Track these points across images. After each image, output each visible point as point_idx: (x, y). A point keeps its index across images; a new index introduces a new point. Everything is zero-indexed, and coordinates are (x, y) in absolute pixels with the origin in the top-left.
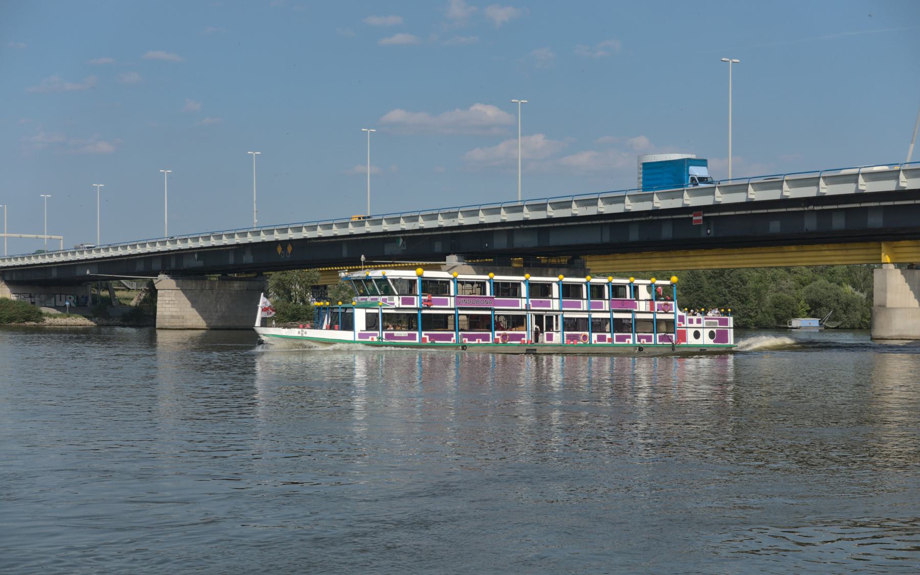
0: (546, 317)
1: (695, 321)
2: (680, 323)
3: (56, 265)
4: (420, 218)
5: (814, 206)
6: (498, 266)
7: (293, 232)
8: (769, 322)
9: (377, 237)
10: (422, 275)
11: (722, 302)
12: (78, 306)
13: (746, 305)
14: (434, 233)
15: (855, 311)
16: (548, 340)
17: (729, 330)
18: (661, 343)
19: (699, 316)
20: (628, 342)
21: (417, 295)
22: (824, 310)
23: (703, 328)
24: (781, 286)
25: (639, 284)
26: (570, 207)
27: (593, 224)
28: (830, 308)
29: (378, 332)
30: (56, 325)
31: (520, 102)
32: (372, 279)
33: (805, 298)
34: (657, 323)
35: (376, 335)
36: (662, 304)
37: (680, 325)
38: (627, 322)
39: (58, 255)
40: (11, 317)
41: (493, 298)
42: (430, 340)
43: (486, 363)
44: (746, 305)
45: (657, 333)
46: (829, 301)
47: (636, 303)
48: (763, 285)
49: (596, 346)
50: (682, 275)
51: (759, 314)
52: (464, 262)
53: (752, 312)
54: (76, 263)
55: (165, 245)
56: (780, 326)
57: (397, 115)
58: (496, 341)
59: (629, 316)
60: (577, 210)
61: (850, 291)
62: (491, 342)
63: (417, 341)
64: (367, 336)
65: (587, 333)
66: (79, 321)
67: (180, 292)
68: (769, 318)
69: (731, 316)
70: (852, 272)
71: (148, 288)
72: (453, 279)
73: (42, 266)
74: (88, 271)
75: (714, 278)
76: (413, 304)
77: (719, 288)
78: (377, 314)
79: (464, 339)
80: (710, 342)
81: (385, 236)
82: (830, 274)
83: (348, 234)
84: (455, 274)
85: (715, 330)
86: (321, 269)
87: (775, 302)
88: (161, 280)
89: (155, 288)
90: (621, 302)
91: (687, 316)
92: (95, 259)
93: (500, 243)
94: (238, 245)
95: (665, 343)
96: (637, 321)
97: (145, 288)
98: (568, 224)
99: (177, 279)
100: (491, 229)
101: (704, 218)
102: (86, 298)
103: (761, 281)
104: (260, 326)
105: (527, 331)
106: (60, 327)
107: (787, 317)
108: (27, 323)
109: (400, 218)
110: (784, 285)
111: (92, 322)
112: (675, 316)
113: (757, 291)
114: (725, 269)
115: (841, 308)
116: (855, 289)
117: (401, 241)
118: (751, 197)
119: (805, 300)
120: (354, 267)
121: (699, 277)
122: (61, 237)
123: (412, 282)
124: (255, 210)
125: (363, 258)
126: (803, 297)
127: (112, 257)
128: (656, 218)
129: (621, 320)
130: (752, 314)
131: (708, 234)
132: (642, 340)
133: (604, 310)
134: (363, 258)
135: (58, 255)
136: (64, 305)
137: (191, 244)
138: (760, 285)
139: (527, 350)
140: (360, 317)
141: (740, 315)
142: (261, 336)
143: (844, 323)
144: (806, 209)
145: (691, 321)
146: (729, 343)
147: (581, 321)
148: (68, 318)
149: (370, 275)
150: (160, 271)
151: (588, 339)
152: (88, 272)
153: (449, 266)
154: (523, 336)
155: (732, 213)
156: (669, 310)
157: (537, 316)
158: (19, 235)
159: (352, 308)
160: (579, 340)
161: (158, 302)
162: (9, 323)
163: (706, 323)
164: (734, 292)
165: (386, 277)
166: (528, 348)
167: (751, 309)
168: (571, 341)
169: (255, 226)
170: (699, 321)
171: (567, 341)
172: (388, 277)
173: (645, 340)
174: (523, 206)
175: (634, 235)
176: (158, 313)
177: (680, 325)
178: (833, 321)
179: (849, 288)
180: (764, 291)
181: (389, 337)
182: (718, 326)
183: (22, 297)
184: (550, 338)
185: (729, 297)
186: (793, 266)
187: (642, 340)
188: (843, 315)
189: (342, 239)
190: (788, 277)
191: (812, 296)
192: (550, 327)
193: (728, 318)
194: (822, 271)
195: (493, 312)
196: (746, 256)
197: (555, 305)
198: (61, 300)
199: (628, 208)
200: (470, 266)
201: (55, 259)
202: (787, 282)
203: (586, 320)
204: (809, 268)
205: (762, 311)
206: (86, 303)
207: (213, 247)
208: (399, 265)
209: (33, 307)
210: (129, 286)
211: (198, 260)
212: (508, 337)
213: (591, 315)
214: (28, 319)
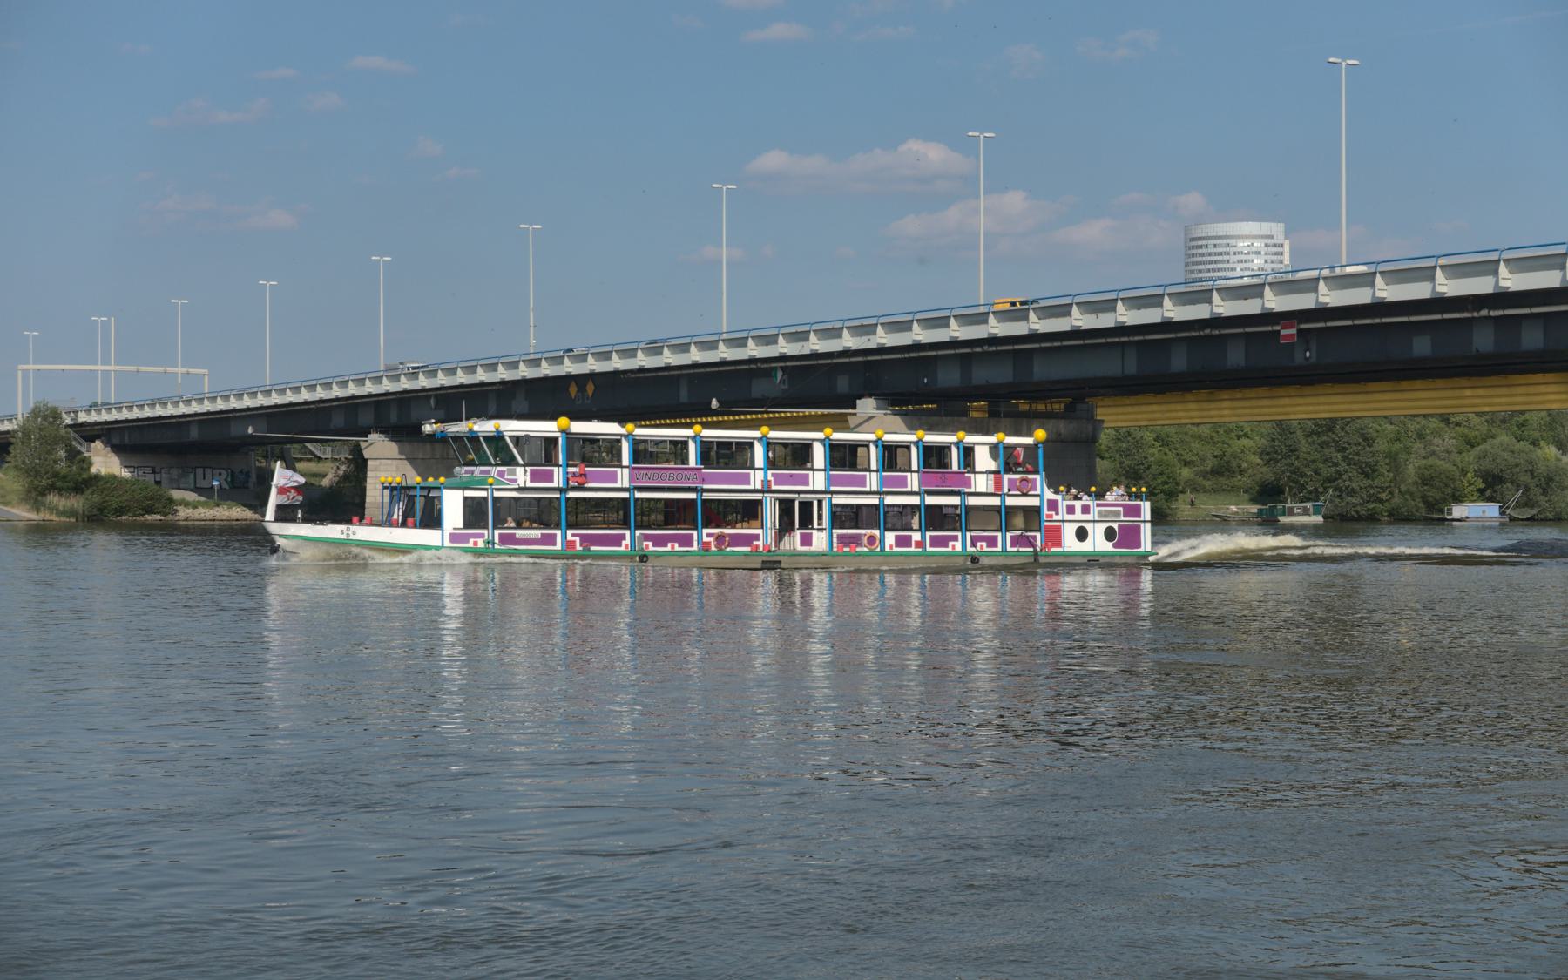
0: (800, 502)
1: (1078, 509)
2: (1050, 513)
3: (196, 418)
4: (845, 331)
5: (1490, 309)
6: (946, 416)
7: (596, 361)
8: (1414, 510)
9: (804, 363)
10: (569, 428)
11: (1331, 475)
12: (235, 487)
13: (1373, 480)
14: (835, 361)
15: (1562, 490)
16: (803, 544)
17: (1142, 524)
18: (1015, 549)
19: (1086, 500)
20: (954, 547)
21: (559, 466)
22: (1507, 488)
23: (1094, 521)
24: (1432, 448)
25: (974, 444)
26: (1069, 314)
27: (1108, 343)
28: (1518, 485)
29: (485, 532)
30: (197, 520)
31: (982, 136)
32: (478, 437)
33: (1476, 468)
34: (1006, 513)
35: (482, 536)
36: (1016, 480)
37: (1051, 516)
38: (950, 511)
39: (200, 401)
40: (122, 507)
41: (701, 469)
42: (581, 545)
43: (684, 585)
44: (1373, 480)
45: (1007, 530)
46: (1518, 473)
47: (970, 478)
48: (1402, 445)
49: (892, 554)
50: (1263, 430)
51: (1396, 495)
52: (887, 409)
53: (1384, 492)
54: (231, 415)
55: (381, 383)
56: (1432, 515)
57: (773, 160)
58: (705, 547)
59: (955, 500)
60: (1081, 320)
61: (1553, 455)
62: (695, 547)
63: (558, 546)
64: (465, 538)
65: (876, 532)
66: (235, 514)
67: (406, 462)
68: (1413, 503)
69: (1146, 500)
70: (1556, 423)
71: (351, 457)
72: (626, 436)
73: (174, 420)
74: (250, 428)
75: (1318, 434)
76: (552, 481)
77: (1326, 451)
78: (485, 499)
79: (645, 543)
80: (1108, 546)
81: (753, 366)
82: (1517, 426)
83: (690, 363)
84: (880, 433)
85: (1115, 526)
86: (704, 420)
87: (1423, 474)
88: (372, 444)
89: (362, 455)
90: (940, 475)
91: (1063, 500)
92: (262, 408)
93: (949, 377)
94: (503, 383)
95: (1021, 549)
96: (969, 509)
97: (347, 456)
98: (1066, 343)
99: (399, 441)
100: (934, 353)
101: (1299, 331)
102: (248, 474)
103: (1399, 440)
104: (273, 520)
105: (762, 528)
106: (203, 522)
107: (1445, 501)
108: (149, 517)
109: (777, 335)
110: (1438, 446)
111: (257, 515)
112: (1042, 501)
113: (1392, 457)
114: (1337, 419)
115: (1537, 486)
116: (1561, 452)
117: (780, 374)
118: (1380, 294)
119: (1475, 471)
120: (683, 421)
121: (1291, 433)
122: (206, 371)
123: (550, 442)
124: (532, 324)
125: (714, 403)
126: (1472, 467)
127: (291, 404)
128: (1217, 332)
129: (940, 507)
130: (1384, 496)
131: (1307, 359)
132: (979, 544)
133: (910, 490)
134: (714, 403)
135: (200, 401)
136: (210, 486)
137: (423, 382)
138: (1397, 445)
139: (763, 562)
140: (452, 504)
141: (1362, 498)
142: (277, 538)
143: (1544, 510)
144: (1476, 314)
145: (1071, 510)
146: (1142, 549)
147: (864, 508)
148: (217, 509)
149: (476, 428)
150: (372, 428)
151: (878, 542)
152: (250, 431)
153: (861, 417)
154: (756, 537)
155: (1349, 323)
156: (1030, 490)
157: (781, 501)
158: (135, 368)
159: (439, 488)
160: (860, 545)
161: (369, 480)
162: (118, 516)
163: (1100, 512)
164: (1353, 459)
165: (501, 432)
166: (765, 559)
167: (1381, 488)
168: (846, 546)
169: (532, 351)
170: (1086, 510)
171: (838, 547)
172: (505, 433)
173: (984, 544)
174: (988, 313)
175: (1179, 362)
176: (368, 500)
177: (1051, 516)
178: (1524, 507)
179: (1551, 451)
180: (1403, 456)
181: (505, 539)
182: (1122, 519)
183: (140, 473)
184: (806, 540)
185: (1343, 466)
186: (1453, 414)
187: (979, 544)
188: (1542, 497)
189: (679, 372)
190: (1446, 432)
191: (1487, 464)
192: (806, 522)
193: (1142, 503)
194: (1503, 421)
195: (699, 494)
196: (1322, 399)
197: (818, 481)
198: (204, 478)
199: (1122, 319)
200: (897, 417)
201: (195, 408)
202: (1443, 440)
203: (874, 508)
204: (1481, 416)
205: (1400, 492)
206: (247, 482)
207: (462, 386)
208: (777, 415)
209: (158, 490)
210: (318, 454)
211: (436, 408)
212: (727, 539)
213: (883, 499)
214: (150, 511)
